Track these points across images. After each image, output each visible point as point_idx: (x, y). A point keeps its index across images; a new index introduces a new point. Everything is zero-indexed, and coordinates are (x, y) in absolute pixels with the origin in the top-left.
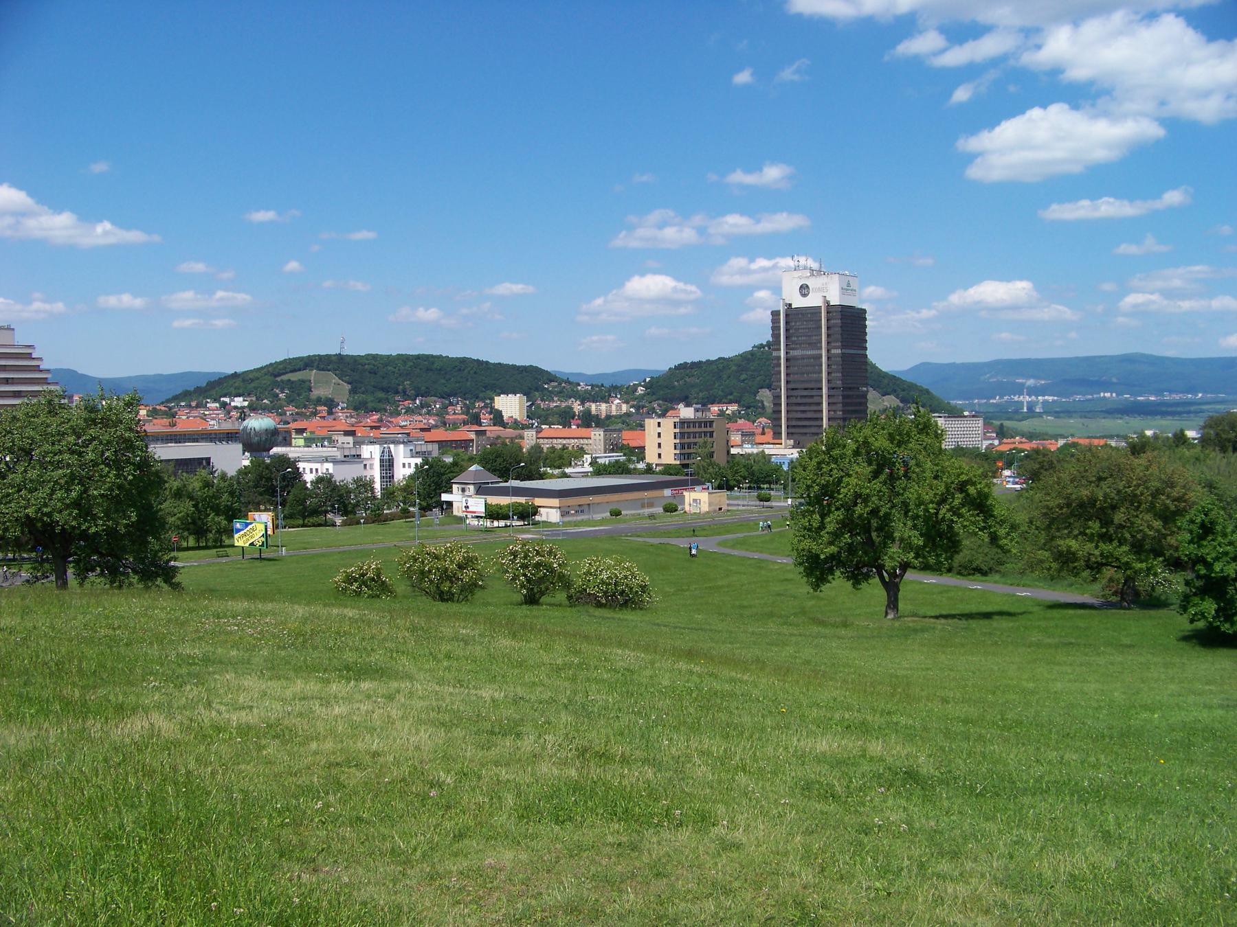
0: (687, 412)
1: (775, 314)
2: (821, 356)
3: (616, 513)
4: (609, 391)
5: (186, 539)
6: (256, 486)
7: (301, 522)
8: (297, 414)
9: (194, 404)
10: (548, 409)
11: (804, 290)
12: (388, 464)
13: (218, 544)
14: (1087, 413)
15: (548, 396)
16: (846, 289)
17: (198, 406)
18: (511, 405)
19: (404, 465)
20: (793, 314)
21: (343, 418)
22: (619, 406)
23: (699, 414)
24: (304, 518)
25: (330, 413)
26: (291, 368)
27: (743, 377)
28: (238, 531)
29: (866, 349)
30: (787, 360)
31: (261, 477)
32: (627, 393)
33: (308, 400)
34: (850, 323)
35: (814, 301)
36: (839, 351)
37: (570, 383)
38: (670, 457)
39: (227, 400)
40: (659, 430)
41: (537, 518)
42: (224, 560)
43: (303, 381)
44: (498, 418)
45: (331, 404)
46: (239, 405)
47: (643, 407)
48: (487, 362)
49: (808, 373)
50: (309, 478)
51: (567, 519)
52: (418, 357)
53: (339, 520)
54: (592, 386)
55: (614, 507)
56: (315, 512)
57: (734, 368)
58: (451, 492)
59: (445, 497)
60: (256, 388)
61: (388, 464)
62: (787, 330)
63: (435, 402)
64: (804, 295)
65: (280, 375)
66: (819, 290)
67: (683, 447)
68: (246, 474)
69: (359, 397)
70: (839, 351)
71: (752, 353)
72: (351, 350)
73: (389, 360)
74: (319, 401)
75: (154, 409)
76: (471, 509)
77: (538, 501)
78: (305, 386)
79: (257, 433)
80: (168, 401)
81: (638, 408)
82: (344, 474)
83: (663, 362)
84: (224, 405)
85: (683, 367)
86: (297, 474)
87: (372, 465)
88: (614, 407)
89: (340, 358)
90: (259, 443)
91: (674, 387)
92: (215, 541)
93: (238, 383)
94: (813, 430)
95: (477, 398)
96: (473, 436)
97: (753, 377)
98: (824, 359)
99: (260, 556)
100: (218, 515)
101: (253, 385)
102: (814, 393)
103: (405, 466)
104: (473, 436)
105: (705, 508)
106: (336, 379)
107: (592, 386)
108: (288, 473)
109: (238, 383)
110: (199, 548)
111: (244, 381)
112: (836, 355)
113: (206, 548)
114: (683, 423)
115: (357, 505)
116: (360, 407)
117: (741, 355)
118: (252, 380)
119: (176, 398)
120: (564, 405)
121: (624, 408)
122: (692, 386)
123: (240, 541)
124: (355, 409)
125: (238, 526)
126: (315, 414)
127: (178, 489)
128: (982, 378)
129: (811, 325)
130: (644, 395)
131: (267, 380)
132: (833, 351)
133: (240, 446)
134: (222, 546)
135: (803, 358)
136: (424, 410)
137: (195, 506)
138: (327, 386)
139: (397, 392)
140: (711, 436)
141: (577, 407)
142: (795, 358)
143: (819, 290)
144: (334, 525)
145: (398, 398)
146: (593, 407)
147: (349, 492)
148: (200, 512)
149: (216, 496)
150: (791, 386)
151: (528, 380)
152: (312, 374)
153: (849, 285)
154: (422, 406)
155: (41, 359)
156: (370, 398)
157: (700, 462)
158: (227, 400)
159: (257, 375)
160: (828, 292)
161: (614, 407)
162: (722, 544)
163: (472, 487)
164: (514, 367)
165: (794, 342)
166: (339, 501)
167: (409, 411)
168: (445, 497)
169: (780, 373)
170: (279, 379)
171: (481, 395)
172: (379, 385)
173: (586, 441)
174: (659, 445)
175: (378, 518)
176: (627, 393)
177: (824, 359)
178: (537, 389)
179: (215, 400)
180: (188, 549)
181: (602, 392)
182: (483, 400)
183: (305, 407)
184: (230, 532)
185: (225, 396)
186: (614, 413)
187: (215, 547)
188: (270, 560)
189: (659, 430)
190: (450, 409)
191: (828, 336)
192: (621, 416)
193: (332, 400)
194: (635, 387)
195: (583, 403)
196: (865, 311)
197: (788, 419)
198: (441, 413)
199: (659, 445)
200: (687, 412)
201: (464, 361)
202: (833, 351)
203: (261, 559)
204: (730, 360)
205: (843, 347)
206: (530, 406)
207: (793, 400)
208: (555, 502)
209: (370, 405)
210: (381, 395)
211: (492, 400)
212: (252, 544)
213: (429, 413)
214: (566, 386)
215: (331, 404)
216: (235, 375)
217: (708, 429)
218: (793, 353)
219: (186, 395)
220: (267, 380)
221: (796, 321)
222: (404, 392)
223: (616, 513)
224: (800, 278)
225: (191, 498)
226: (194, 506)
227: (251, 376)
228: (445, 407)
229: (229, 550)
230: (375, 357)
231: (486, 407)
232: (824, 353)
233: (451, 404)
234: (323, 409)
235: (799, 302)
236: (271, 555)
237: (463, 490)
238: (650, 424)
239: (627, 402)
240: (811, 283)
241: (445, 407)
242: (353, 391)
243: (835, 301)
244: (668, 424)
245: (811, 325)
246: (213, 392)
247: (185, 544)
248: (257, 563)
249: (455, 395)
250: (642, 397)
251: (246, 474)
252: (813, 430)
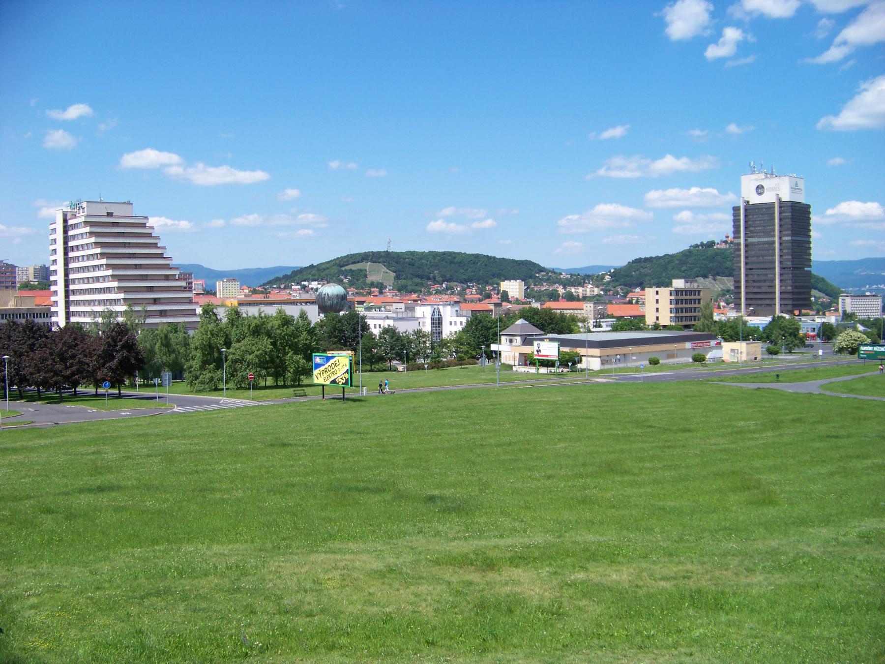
0: (679, 283)
1: (736, 209)
2: (774, 242)
3: (654, 362)
4: (584, 279)
5: (264, 377)
6: (330, 337)
7: (368, 367)
8: (357, 293)
9: (282, 286)
10: (540, 292)
11: (760, 189)
12: (437, 322)
13: (296, 383)
14: (24, 449)
15: (540, 282)
16: (794, 189)
17: (285, 288)
18: (513, 288)
19: (451, 323)
20: (750, 209)
21: (389, 295)
22: (592, 290)
23: (688, 285)
24: (372, 363)
25: (381, 293)
26: (351, 260)
27: (683, 269)
28: (318, 366)
29: (810, 236)
30: (746, 246)
31: (335, 329)
32: (598, 280)
33: (365, 284)
34: (798, 217)
35: (768, 198)
36: (789, 238)
37: (555, 273)
38: (666, 319)
39: (306, 283)
40: (657, 297)
41: (579, 366)
42: (302, 400)
43: (361, 270)
44: (505, 297)
45: (381, 287)
46: (315, 287)
47: (610, 290)
48: (494, 258)
49: (763, 256)
50: (376, 332)
51: (607, 367)
52: (444, 253)
53: (400, 368)
54: (571, 275)
55: (653, 356)
56: (381, 359)
57: (677, 262)
58: (500, 343)
59: (494, 347)
60: (327, 275)
61: (437, 322)
62: (746, 222)
63: (457, 286)
64: (760, 194)
65: (344, 266)
66: (773, 189)
67: (677, 312)
68: (322, 326)
69: (402, 282)
70: (789, 238)
71: (689, 251)
72: (395, 248)
73: (422, 256)
74: (372, 285)
75: (254, 290)
76: (542, 353)
77: (581, 351)
78: (363, 274)
79: (329, 298)
80: (264, 284)
81: (605, 291)
82: (405, 328)
83: (621, 261)
84: (304, 287)
85: (638, 261)
86: (365, 327)
87: (424, 323)
88: (588, 291)
89: (387, 253)
90: (331, 306)
91: (632, 276)
92: (294, 380)
93: (314, 271)
94: (768, 302)
95: (487, 283)
96: (492, 307)
97: (691, 269)
98: (777, 245)
99: (343, 396)
100: (295, 353)
101: (325, 273)
102: (768, 272)
103: (454, 323)
104: (492, 307)
105: (744, 357)
106: (384, 269)
107: (571, 275)
108: (359, 325)
109: (314, 271)
110: (277, 387)
111: (318, 270)
112: (787, 242)
113: (285, 387)
114: (678, 292)
115: (415, 354)
116: (402, 289)
117: (682, 252)
118: (324, 269)
119: (270, 283)
120: (551, 288)
121: (596, 291)
122: (646, 275)
123: (319, 377)
124: (399, 290)
125: (318, 360)
126: (370, 293)
127: (256, 326)
128: (855, 272)
129: (766, 217)
130: (610, 282)
131: (335, 270)
132: (784, 238)
133: (317, 307)
134: (299, 386)
135: (759, 243)
136: (449, 292)
137: (274, 344)
138: (378, 274)
139: (429, 279)
140: (699, 303)
141: (561, 290)
142: (753, 244)
143: (773, 189)
144: (396, 370)
145: (429, 283)
146: (573, 290)
147: (410, 342)
148: (278, 350)
149: (294, 335)
150: (749, 267)
151: (526, 271)
152: (368, 266)
153: (797, 185)
154: (447, 289)
155: (164, 248)
156: (409, 282)
157: (693, 322)
158: (306, 283)
159: (327, 266)
160: (779, 190)
161: (588, 291)
162: (217, 403)
163: (519, 338)
164: (514, 261)
165: (751, 232)
166: (400, 349)
167: (438, 292)
168: (494, 347)
169: (740, 256)
170: (343, 269)
171: (490, 281)
172: (418, 272)
173: (579, 312)
174: (657, 310)
175: (437, 365)
176: (598, 280)
177: (777, 245)
178: (531, 277)
179: (298, 284)
180: (266, 388)
181: (578, 279)
182: (491, 284)
183: (362, 288)
184: (309, 372)
185: (305, 281)
186: (588, 295)
187: (293, 386)
188: (354, 400)
189: (657, 297)
190: (468, 291)
191: (780, 226)
192: (594, 297)
193: (382, 284)
194: (603, 276)
195: (564, 288)
196: (808, 206)
197: (747, 293)
198: (462, 294)
199: (657, 310)
200: (679, 283)
201: (477, 256)
202: (784, 238)
203: (344, 399)
204: (672, 256)
205: (793, 235)
206: (526, 290)
207: (751, 277)
208: (596, 352)
209: (409, 288)
210: (418, 280)
211: (499, 285)
212: (334, 382)
213: (452, 293)
214: (553, 276)
215: (381, 287)
216: (312, 266)
217: (697, 297)
218: (750, 240)
219: (277, 280)
220: (335, 270)
221: (753, 217)
222: (434, 278)
223: (654, 362)
224: (756, 180)
225: (270, 336)
226: (272, 344)
227: (323, 266)
228: (464, 290)
229: (308, 390)
230: (412, 253)
231: (494, 289)
232: (777, 239)
233: (469, 287)
234: (376, 290)
235: (755, 199)
236: (353, 396)
237: (511, 341)
238: (650, 292)
239: (597, 287)
240: (766, 184)
241: (464, 290)
242: (397, 278)
243: (786, 198)
244: (665, 292)
245: (766, 217)
246: (296, 278)
247: (262, 384)
248: (340, 404)
249: (471, 281)
250: (608, 283)
251: (322, 326)
252: (768, 302)
